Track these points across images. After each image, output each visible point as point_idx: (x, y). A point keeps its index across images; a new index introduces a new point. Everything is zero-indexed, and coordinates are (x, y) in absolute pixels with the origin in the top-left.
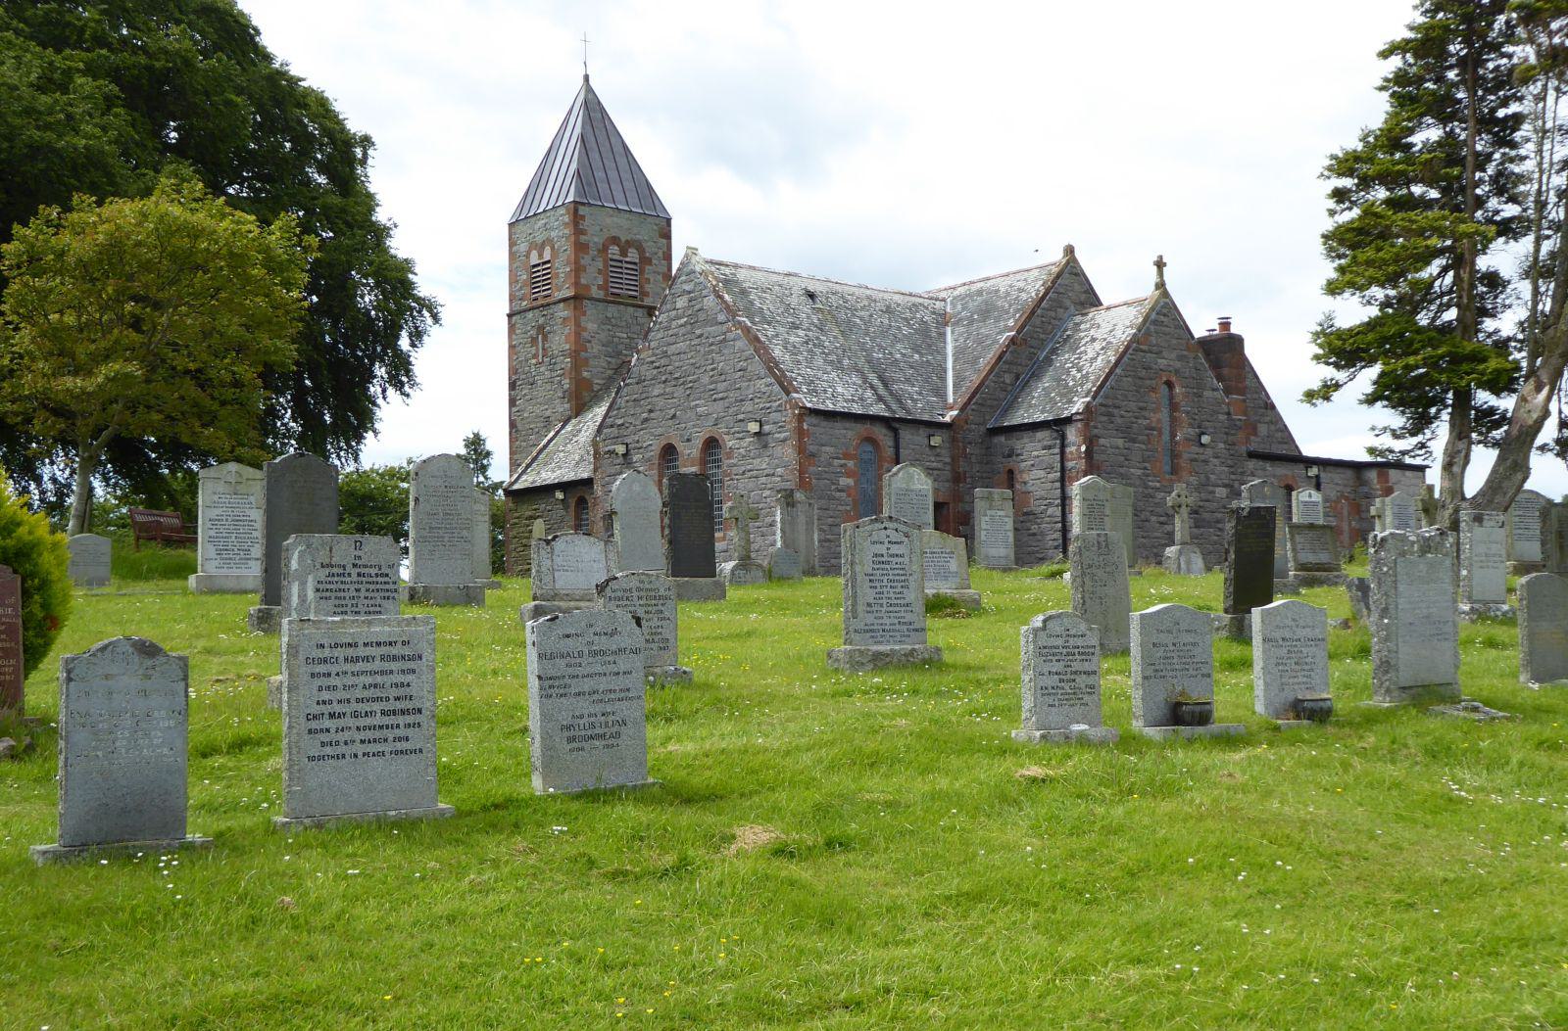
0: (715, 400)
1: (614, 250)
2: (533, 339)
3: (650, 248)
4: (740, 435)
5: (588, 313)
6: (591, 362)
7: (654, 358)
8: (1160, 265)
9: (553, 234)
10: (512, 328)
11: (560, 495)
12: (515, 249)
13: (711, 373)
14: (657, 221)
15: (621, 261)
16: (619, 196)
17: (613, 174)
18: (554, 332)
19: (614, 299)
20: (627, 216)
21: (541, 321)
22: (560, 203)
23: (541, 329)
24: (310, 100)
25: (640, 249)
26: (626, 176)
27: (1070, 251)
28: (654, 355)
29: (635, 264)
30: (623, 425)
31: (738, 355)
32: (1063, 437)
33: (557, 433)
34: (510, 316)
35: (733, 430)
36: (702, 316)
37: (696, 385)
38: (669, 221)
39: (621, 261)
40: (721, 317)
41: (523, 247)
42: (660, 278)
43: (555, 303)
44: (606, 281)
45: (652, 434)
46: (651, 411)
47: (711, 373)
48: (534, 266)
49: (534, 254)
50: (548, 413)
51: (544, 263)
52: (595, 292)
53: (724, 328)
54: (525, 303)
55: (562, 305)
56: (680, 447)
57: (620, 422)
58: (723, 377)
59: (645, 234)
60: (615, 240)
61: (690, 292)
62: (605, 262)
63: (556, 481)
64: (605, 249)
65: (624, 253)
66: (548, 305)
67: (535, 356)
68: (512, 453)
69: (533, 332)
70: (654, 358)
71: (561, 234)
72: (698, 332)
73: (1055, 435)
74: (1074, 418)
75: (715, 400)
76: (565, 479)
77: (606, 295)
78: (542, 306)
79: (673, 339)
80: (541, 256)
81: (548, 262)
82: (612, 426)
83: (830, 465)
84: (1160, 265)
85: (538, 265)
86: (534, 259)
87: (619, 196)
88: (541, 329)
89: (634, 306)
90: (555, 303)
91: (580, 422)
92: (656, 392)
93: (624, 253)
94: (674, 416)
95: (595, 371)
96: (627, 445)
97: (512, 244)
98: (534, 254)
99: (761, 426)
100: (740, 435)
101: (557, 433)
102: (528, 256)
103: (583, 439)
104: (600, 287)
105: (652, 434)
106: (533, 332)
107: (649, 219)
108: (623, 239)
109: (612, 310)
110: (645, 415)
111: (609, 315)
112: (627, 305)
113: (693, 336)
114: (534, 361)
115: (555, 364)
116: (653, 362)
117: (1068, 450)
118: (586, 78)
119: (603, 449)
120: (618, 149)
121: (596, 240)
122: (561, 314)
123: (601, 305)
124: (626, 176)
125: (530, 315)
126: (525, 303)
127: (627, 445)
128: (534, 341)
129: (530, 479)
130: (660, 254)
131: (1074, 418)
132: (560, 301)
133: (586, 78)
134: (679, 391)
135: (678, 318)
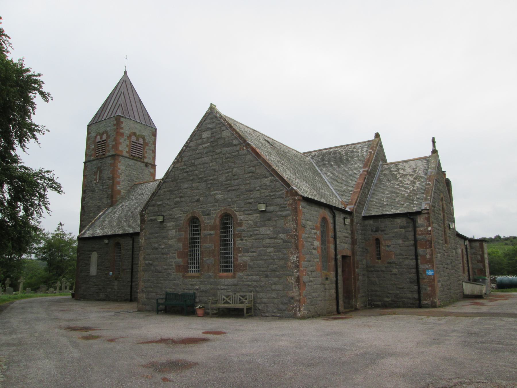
0: (229, 191)
1: (134, 139)
2: (95, 172)
3: (148, 139)
4: (250, 212)
5: (122, 162)
6: (121, 183)
7: (185, 167)
8: (434, 142)
9: (108, 129)
10: (85, 168)
11: (106, 241)
12: (90, 135)
13: (227, 175)
14: (151, 129)
15: (136, 143)
16: (137, 117)
17: (135, 108)
18: (105, 169)
19: (133, 158)
20: (140, 125)
21: (99, 165)
22: (112, 116)
23: (99, 168)
24: (43, 286)
25: (144, 139)
26: (140, 110)
27: (377, 135)
28: (185, 165)
29: (141, 145)
30: (161, 205)
31: (249, 163)
32: (414, 222)
33: (104, 213)
34: (85, 163)
35: (243, 209)
36: (221, 142)
37: (215, 182)
38: (156, 129)
39: (136, 143)
40: (235, 142)
41: (93, 135)
42: (151, 152)
43: (106, 157)
44: (129, 150)
45: (182, 210)
46: (181, 197)
47: (227, 175)
48: (98, 142)
49: (99, 137)
50: (100, 204)
51: (103, 141)
52: (124, 154)
53: (238, 148)
54: (93, 157)
55: (110, 158)
56: (202, 218)
57: (159, 203)
58: (236, 177)
59: (146, 133)
60: (134, 134)
61: (212, 129)
62: (130, 142)
63: (105, 234)
64: (129, 137)
65: (138, 139)
66: (103, 158)
67: (96, 180)
68: (81, 221)
69: (95, 170)
70: (185, 167)
71: (112, 128)
72: (218, 151)
73: (409, 220)
74: (423, 212)
75: (229, 191)
76: (110, 233)
77: (130, 155)
78: (101, 158)
79: (200, 155)
80: (101, 138)
81: (105, 140)
82: (154, 205)
83: (310, 233)
84: (434, 142)
85: (100, 142)
86: (98, 139)
87: (137, 117)
88: (99, 168)
89: (140, 161)
90: (106, 157)
91: (115, 208)
92: (186, 186)
93: (138, 139)
94: (198, 200)
95: (122, 187)
96: (164, 216)
97: (89, 133)
98: (99, 137)
99: (266, 206)
100: (250, 212)
101: (104, 213)
102: (96, 137)
103: (117, 216)
104: (127, 152)
105: (182, 210)
106: (95, 170)
107: (149, 128)
108: (138, 134)
109: (132, 162)
110: (178, 199)
111: (130, 164)
112: (137, 161)
113: (214, 153)
114: (95, 182)
115: (105, 183)
116: (184, 169)
117: (418, 229)
118: (126, 72)
119: (147, 218)
120: (137, 100)
121: (127, 132)
122: (109, 162)
123: (127, 159)
124: (140, 110)
125: (94, 162)
126: (93, 157)
127: (164, 216)
128: (95, 173)
129: (91, 233)
130: (152, 142)
131: (423, 212)
132: (109, 156)
133: (126, 72)
134: (203, 185)
135: (203, 143)
